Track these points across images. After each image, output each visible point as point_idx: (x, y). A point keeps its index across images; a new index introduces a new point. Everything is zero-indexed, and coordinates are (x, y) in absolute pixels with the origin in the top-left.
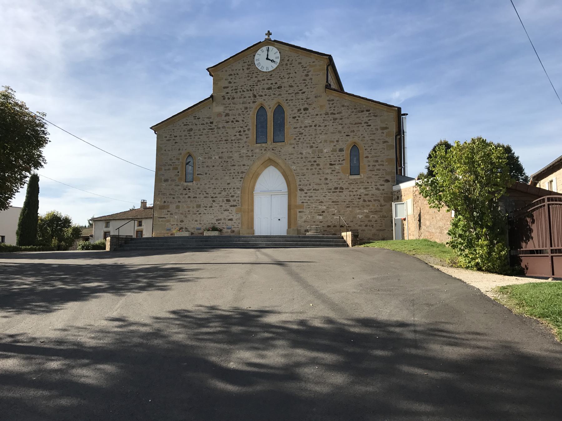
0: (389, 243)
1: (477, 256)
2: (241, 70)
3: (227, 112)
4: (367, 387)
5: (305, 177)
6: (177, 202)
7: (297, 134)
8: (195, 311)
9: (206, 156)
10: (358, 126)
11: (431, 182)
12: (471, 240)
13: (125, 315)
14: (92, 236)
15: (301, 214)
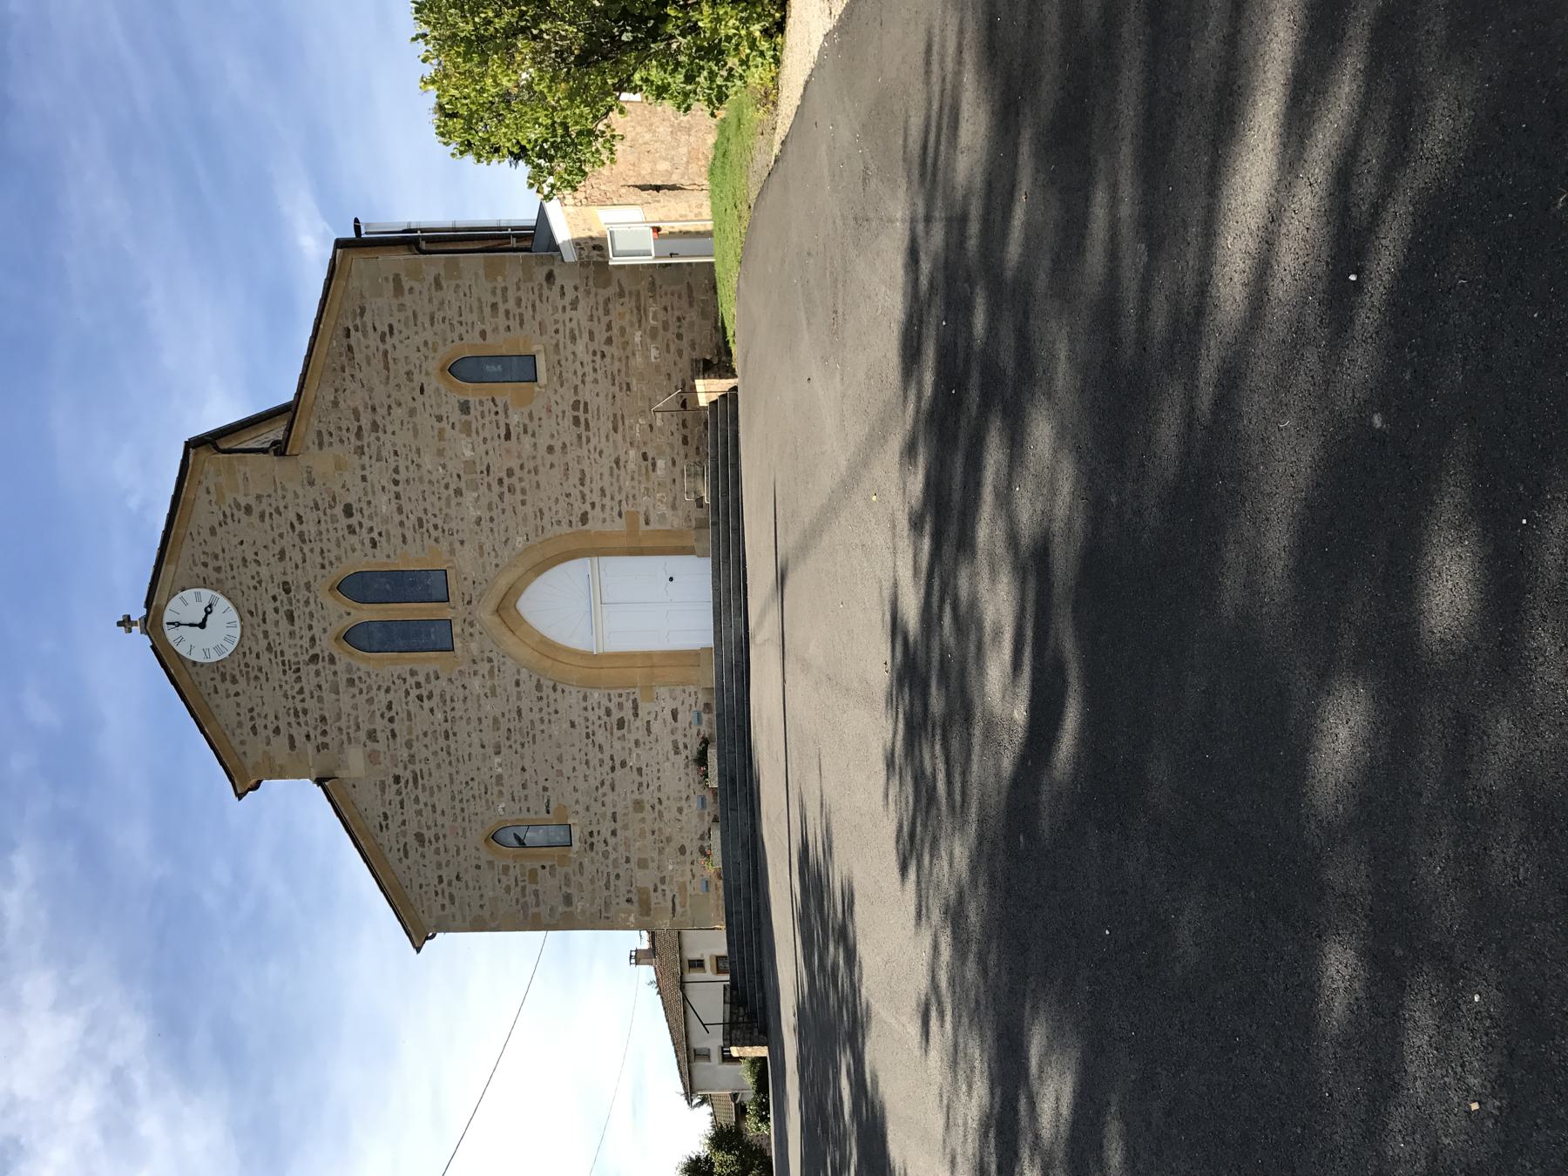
0: (722, 276)
1: (743, 32)
2: (238, 699)
3: (362, 735)
4: (1059, 358)
5: (545, 511)
6: (627, 866)
7: (422, 534)
8: (898, 810)
9: (496, 792)
10: (394, 359)
11: (540, 158)
12: (700, 49)
13: (914, 1004)
14: (734, 1096)
15: (652, 518)
